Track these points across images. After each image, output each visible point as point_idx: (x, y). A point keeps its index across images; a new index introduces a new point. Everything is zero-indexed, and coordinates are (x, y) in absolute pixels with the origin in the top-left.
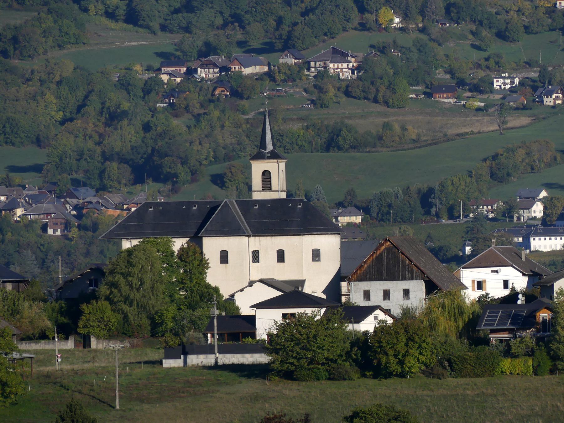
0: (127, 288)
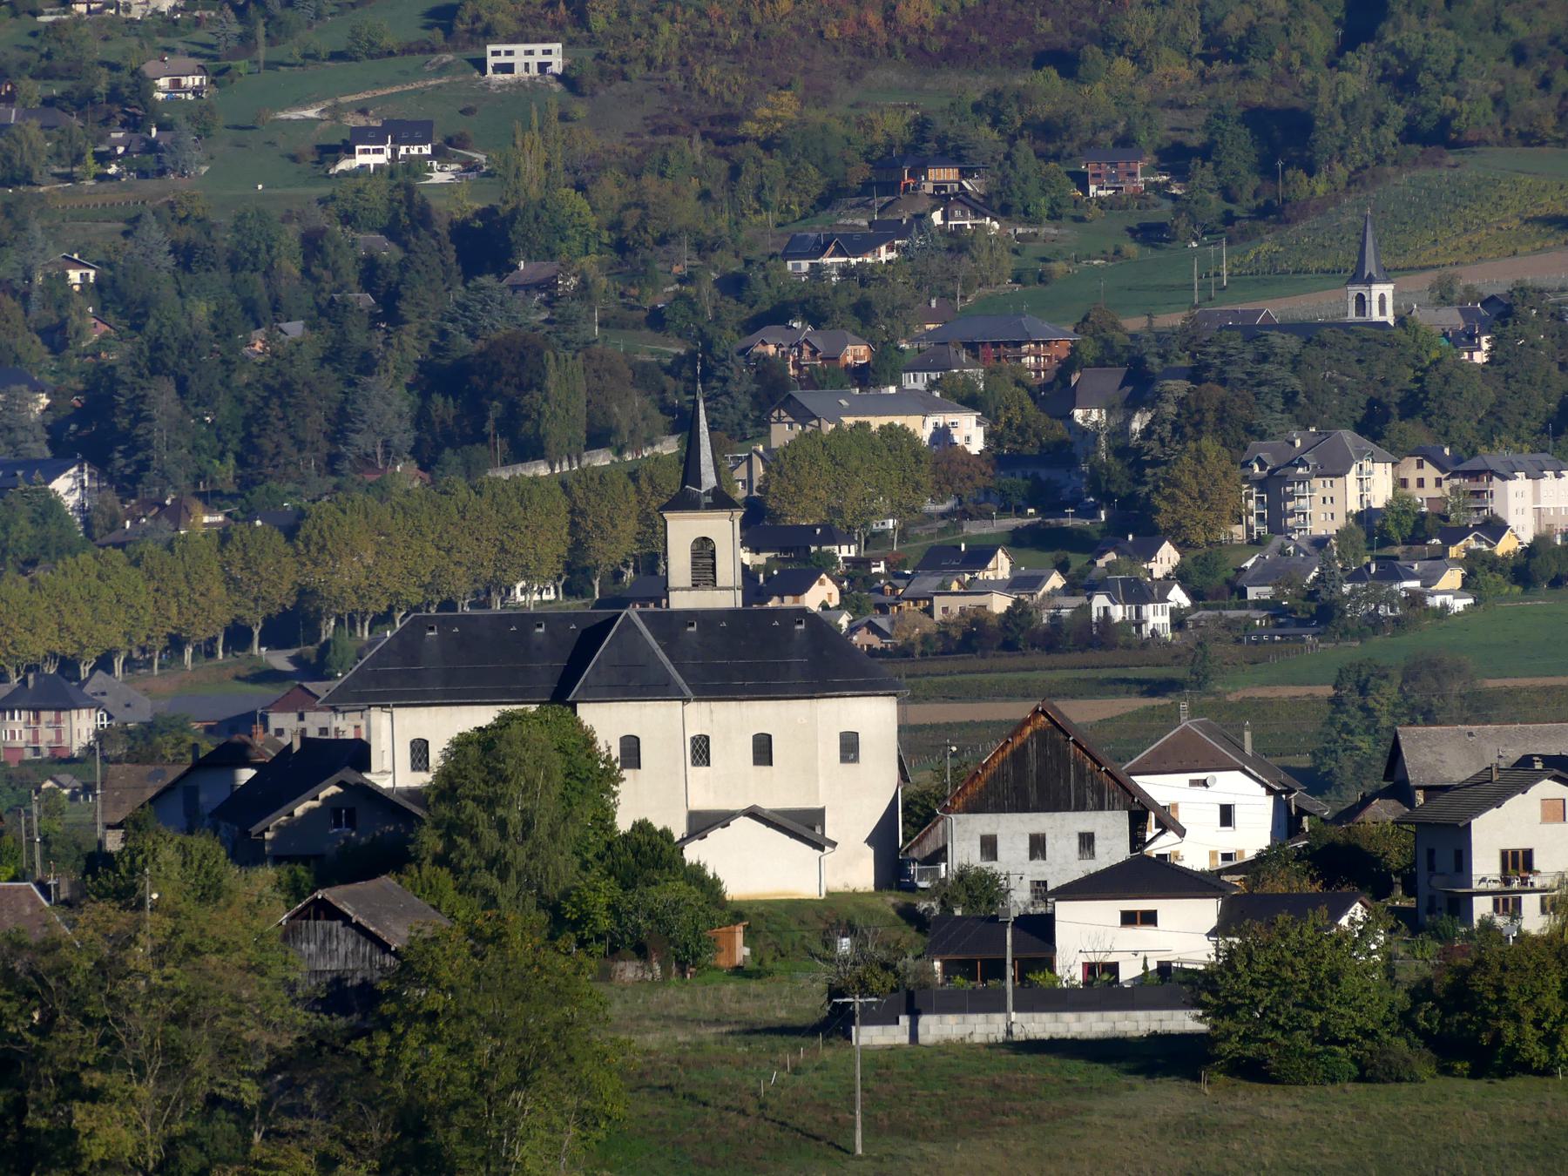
0: (495, 835)
